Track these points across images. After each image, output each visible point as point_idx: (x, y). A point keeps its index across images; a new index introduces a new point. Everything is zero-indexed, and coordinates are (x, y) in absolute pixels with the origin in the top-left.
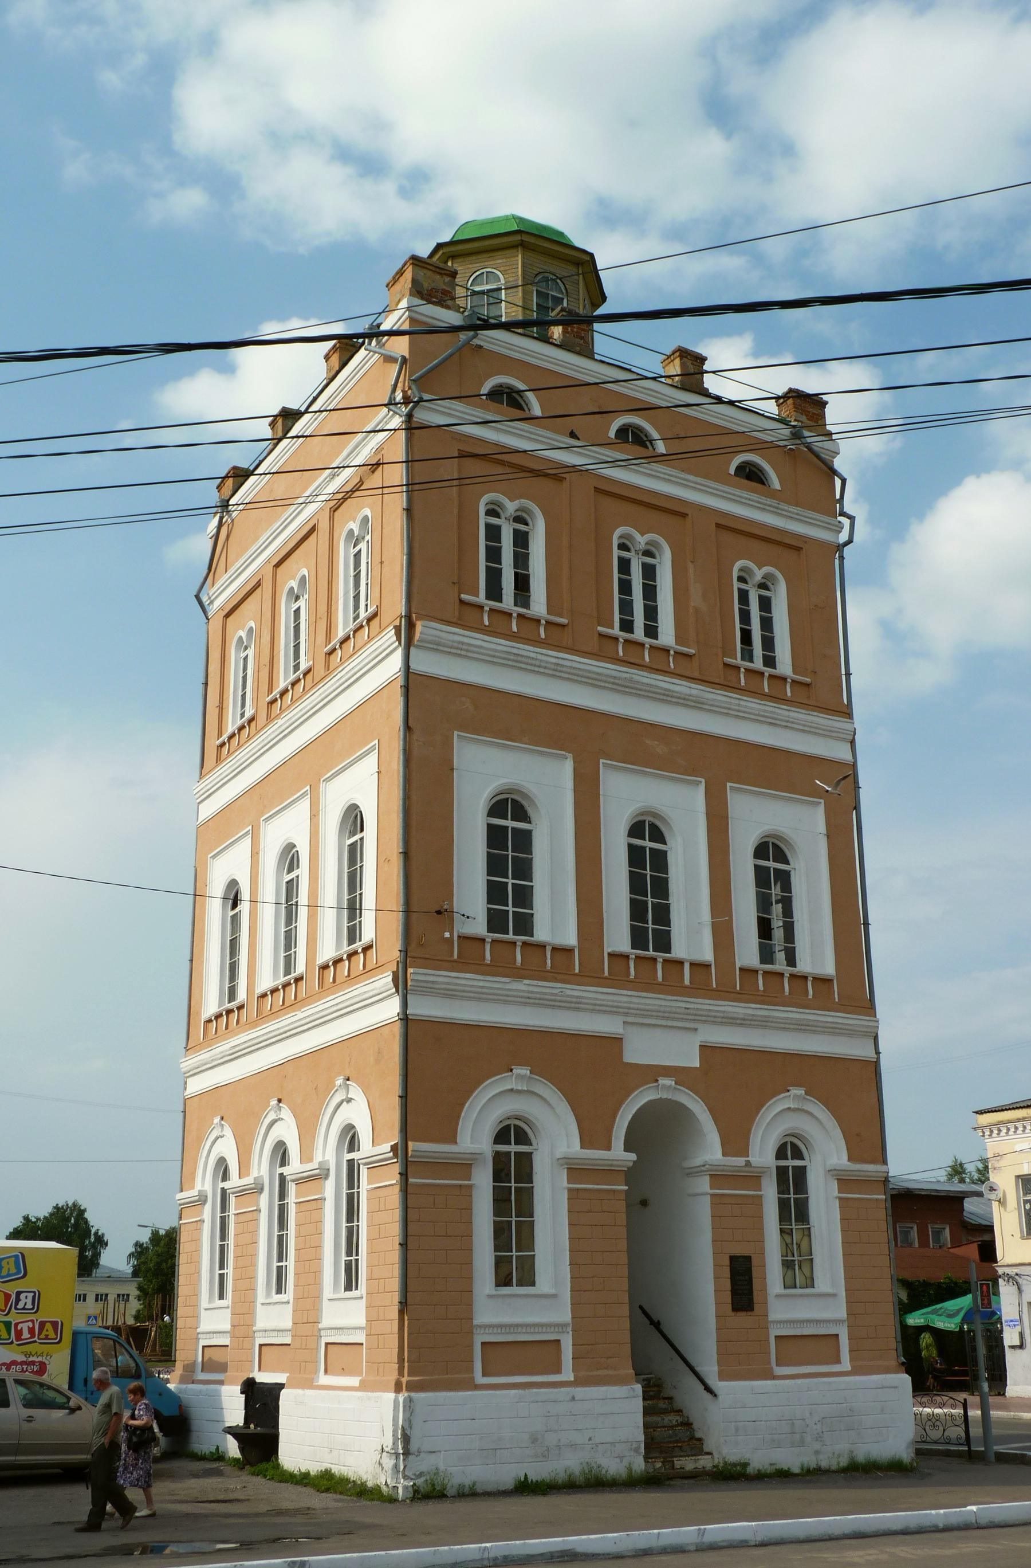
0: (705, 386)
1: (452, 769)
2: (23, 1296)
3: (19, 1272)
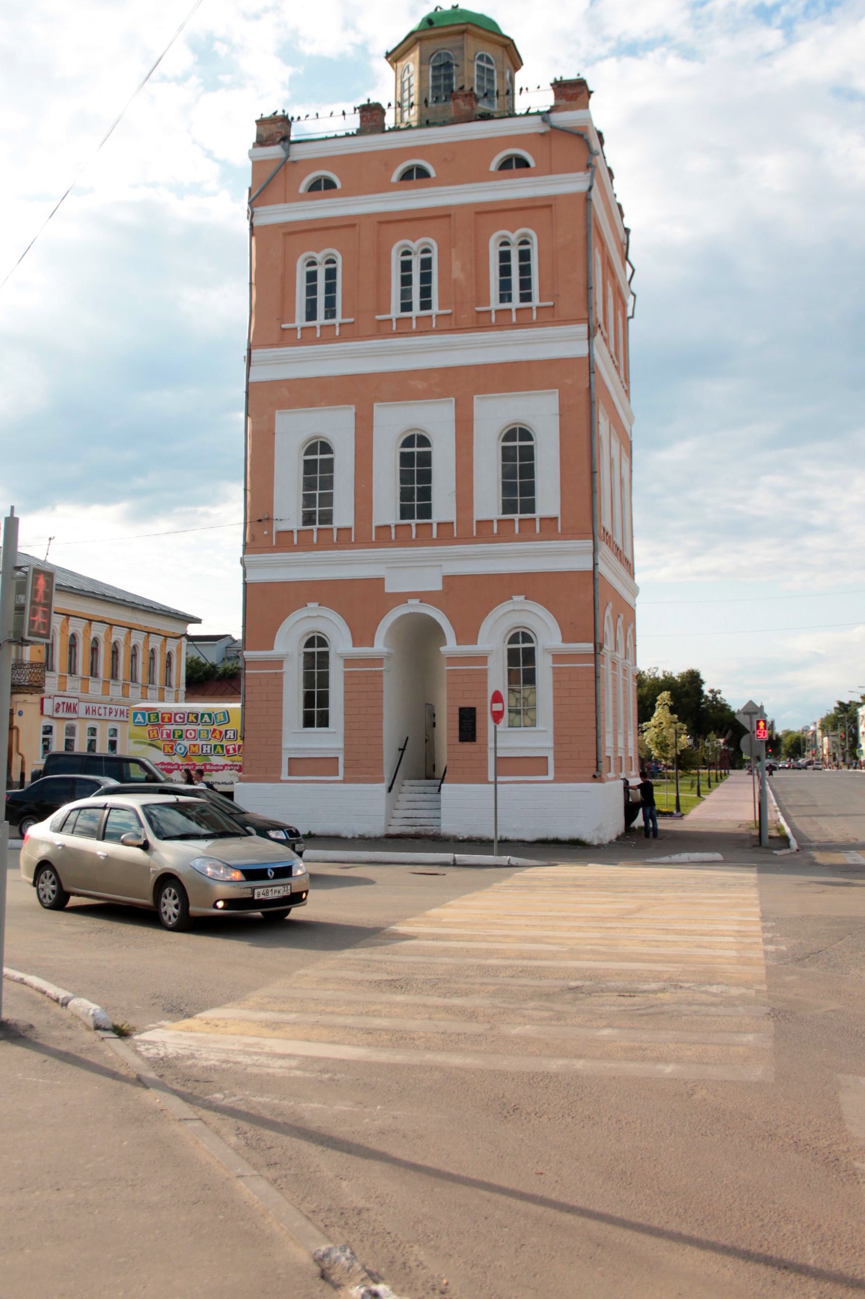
1: (274, 434)
2: (228, 732)
3: (225, 720)
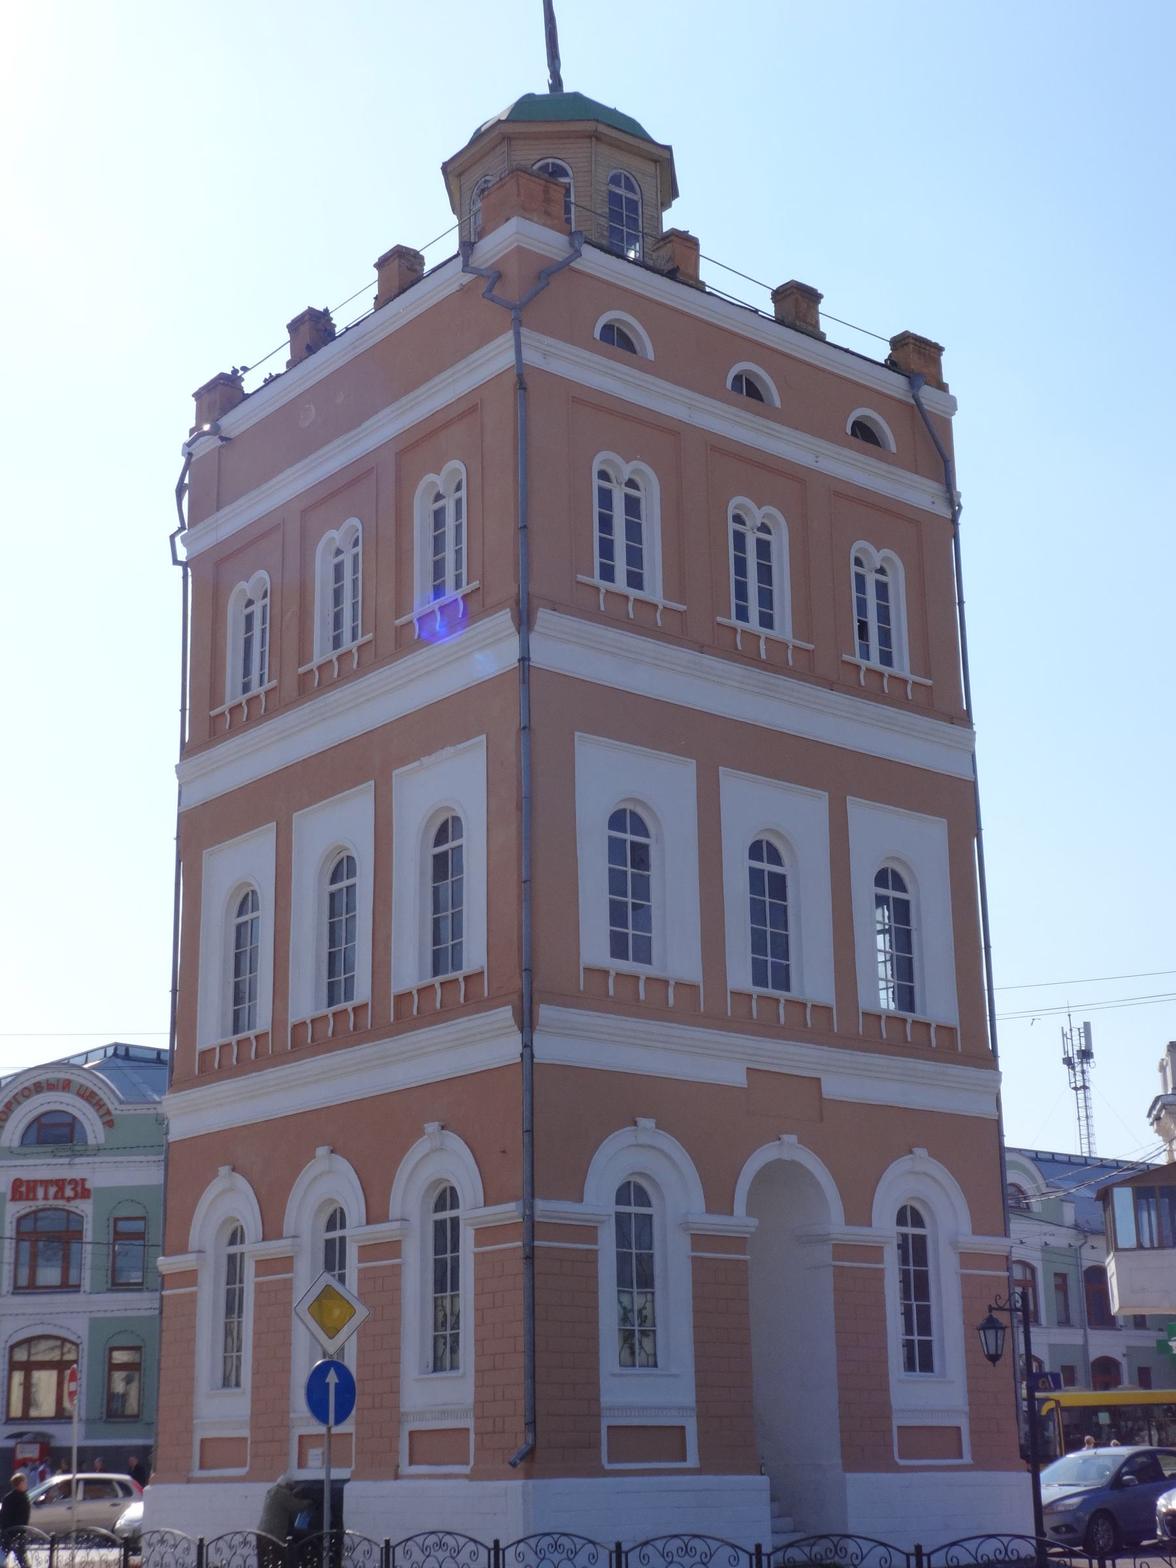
0: (822, 329)
